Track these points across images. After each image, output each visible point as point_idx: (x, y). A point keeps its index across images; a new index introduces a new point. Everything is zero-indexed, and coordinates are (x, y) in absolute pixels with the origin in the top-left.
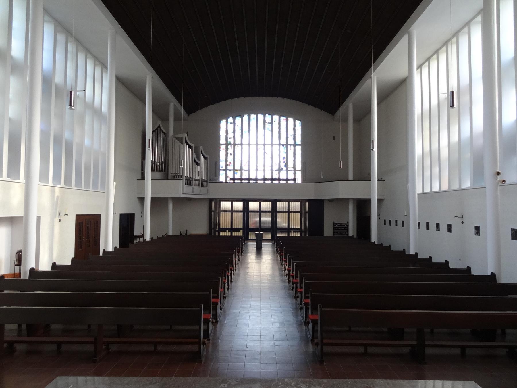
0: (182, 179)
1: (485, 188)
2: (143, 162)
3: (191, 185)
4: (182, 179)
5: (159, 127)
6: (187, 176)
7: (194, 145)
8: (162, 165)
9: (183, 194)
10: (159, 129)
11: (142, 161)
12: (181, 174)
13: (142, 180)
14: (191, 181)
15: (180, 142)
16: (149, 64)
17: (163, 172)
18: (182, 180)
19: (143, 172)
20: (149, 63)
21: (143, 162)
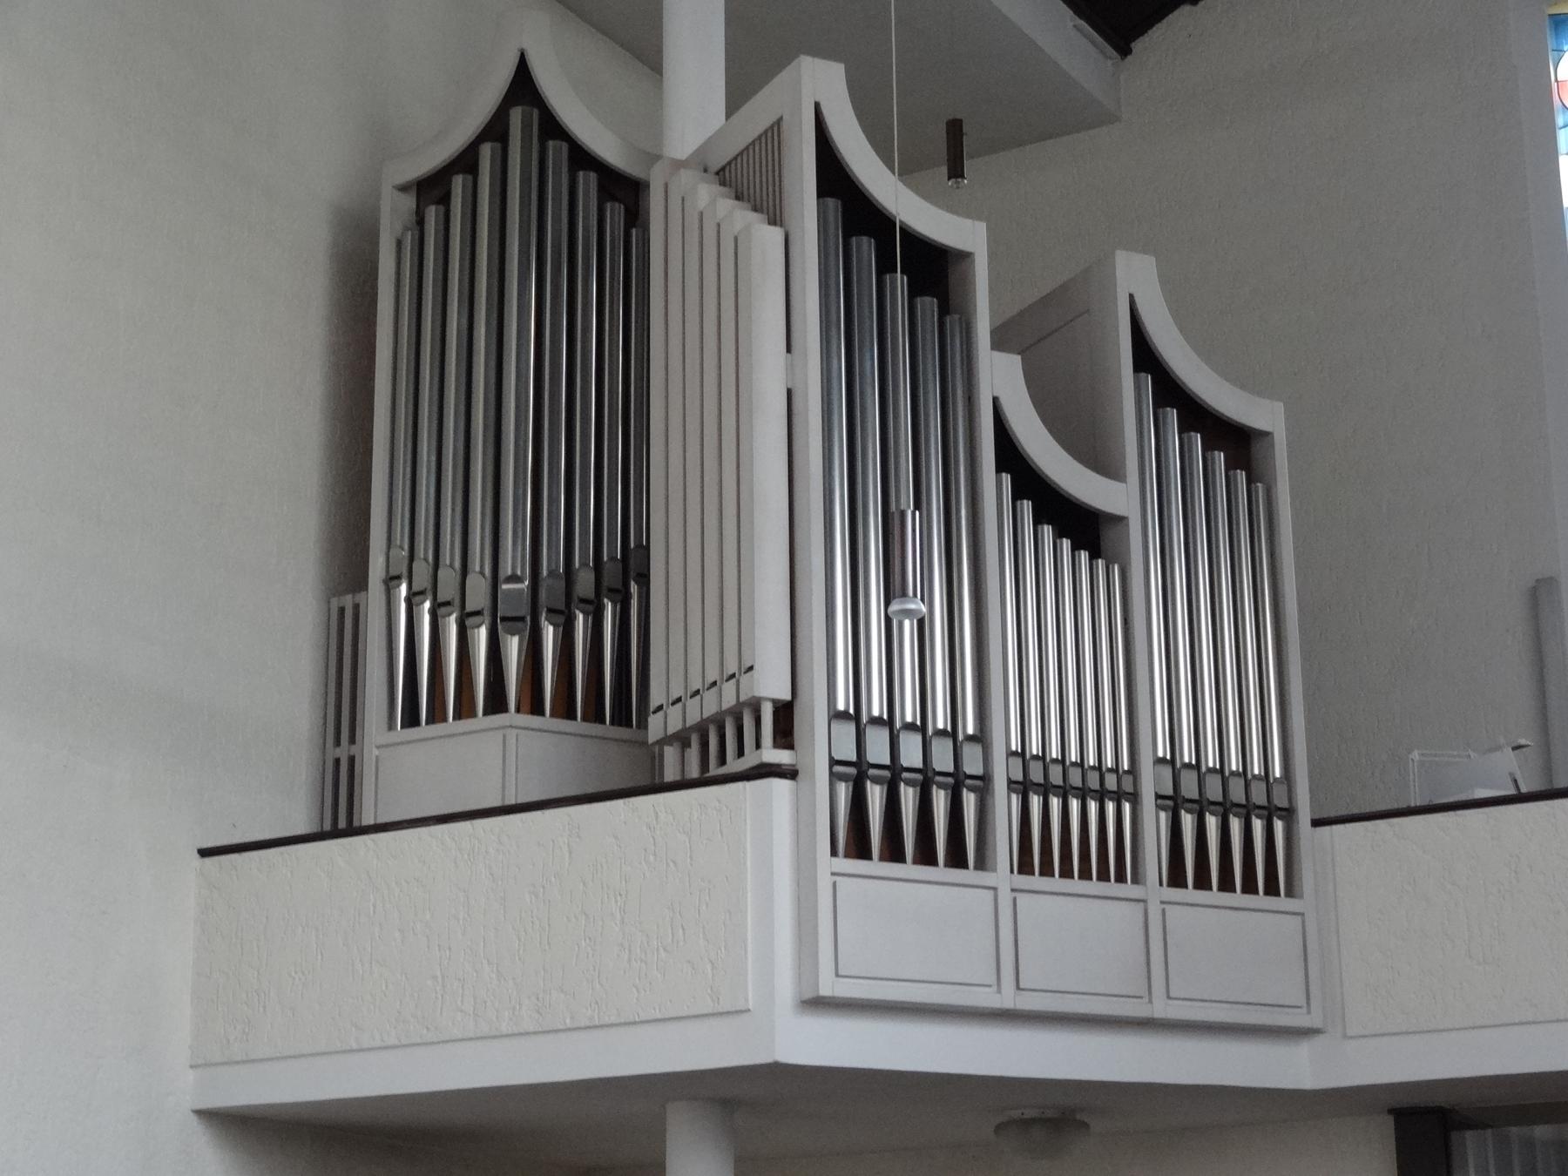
0: (783, 757)
1: (1324, 814)
2: (342, 610)
3: (957, 858)
4: (783, 757)
5: (523, 86)
6: (877, 708)
7: (981, 227)
8: (549, 634)
9: (817, 1004)
10: (516, 115)
11: (335, 603)
12: (772, 684)
13: (335, 834)
14: (1279, 826)
15: (773, 221)
16: (889, 172)
17: (595, 715)
18: (790, 773)
19: (343, 753)
20: (890, 169)
21: (342, 610)
